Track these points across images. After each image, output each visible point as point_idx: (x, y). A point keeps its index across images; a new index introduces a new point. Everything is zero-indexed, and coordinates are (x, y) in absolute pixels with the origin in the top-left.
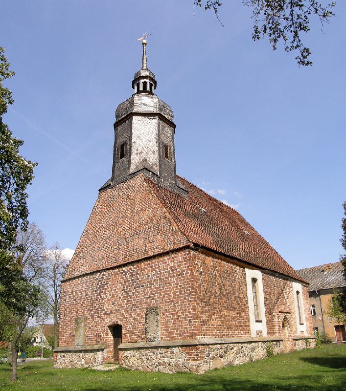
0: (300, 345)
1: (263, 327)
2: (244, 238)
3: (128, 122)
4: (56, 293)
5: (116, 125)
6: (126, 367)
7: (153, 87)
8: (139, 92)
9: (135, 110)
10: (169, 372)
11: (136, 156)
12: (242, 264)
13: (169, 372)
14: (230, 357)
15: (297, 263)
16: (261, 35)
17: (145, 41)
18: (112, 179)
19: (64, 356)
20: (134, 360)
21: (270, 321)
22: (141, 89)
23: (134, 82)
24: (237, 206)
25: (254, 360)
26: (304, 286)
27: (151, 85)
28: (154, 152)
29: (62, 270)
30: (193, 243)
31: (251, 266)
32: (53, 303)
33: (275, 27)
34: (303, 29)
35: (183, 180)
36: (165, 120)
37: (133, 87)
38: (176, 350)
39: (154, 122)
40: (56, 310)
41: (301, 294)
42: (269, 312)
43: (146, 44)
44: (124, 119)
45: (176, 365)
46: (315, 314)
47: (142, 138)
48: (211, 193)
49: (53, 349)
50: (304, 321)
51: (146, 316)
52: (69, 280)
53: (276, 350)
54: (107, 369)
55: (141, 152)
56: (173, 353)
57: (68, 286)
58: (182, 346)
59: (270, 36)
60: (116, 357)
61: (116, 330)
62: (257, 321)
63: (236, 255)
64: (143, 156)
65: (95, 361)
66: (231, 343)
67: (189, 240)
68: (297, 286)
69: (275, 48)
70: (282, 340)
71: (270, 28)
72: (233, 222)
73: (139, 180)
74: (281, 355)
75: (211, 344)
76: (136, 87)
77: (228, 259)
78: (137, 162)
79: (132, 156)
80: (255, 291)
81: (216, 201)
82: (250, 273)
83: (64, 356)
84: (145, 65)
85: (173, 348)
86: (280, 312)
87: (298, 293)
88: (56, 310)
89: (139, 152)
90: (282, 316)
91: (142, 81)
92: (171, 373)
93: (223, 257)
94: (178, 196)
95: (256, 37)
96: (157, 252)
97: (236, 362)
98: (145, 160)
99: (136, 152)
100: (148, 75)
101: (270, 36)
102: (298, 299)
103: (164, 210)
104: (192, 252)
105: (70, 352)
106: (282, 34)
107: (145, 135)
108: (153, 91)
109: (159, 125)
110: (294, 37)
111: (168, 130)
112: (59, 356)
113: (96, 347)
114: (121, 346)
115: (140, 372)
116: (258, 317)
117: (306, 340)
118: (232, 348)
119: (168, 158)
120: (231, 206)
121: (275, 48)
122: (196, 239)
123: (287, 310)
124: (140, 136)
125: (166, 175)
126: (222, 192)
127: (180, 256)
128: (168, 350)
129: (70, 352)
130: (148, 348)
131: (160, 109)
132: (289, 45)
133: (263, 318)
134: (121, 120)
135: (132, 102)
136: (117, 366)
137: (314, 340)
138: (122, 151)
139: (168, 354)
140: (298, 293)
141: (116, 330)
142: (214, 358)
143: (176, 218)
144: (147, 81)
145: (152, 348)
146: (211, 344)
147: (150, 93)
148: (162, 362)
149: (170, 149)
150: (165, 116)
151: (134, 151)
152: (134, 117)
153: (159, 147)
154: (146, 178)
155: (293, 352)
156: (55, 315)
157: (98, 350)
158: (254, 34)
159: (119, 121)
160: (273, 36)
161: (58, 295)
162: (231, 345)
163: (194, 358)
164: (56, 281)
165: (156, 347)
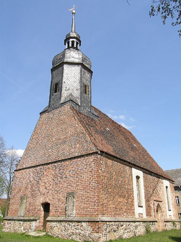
0: (169, 226)
1: (143, 211)
2: (133, 148)
3: (60, 68)
4: (10, 177)
5: (53, 70)
6: (50, 234)
7: (79, 45)
8: (69, 48)
9: (65, 60)
10: (79, 240)
11: (65, 91)
12: (130, 165)
13: (79, 240)
14: (121, 231)
15: (165, 164)
16: (155, 13)
17: (74, 11)
18: (49, 106)
19: (10, 223)
20: (57, 229)
21: (148, 207)
22: (70, 45)
23: (65, 41)
24: (131, 127)
25: (137, 235)
26: (171, 183)
27: (77, 43)
28: (77, 90)
29: (16, 163)
30: (100, 150)
31: (136, 167)
32: (7, 184)
33: (167, 7)
34: (164, 23)
35: (96, 109)
36: (85, 67)
37: (65, 44)
38: (84, 224)
39: (78, 69)
40: (9, 189)
41: (169, 188)
42: (147, 201)
43: (75, 13)
44: (58, 66)
45: (84, 236)
46: (179, 203)
47: (70, 79)
48: (114, 118)
49: (4, 216)
50: (171, 208)
51: (66, 198)
52: (20, 170)
53: (153, 228)
54: (37, 235)
55: (69, 89)
56: (82, 226)
57: (18, 174)
58: (88, 222)
59: (162, 14)
60: (44, 226)
61: (46, 207)
62: (139, 206)
63: (127, 159)
64: (70, 91)
65: (30, 228)
66: (121, 222)
67: (97, 149)
68: (166, 183)
69: (164, 23)
70: (156, 222)
71: (162, 8)
72: (126, 139)
73: (67, 107)
74: (156, 232)
75: (108, 222)
76: (67, 44)
77: (122, 161)
78: (66, 96)
79: (63, 91)
80: (138, 186)
81: (116, 123)
82: (136, 172)
83: (10, 223)
84: (73, 29)
85: (83, 223)
86: (155, 201)
87: (167, 187)
88: (9, 189)
89: (67, 89)
90: (156, 204)
91: (71, 40)
92: (80, 241)
93: (119, 160)
94: (92, 120)
95: (152, 13)
96: (77, 154)
97: (125, 236)
98: (71, 95)
99: (65, 89)
100: (76, 36)
101: (162, 14)
102: (167, 192)
103: (82, 128)
104: (99, 156)
105: (15, 220)
106: (171, 13)
107: (71, 77)
108: (79, 47)
109: (81, 71)
110: (179, 15)
111: (88, 75)
112: (6, 222)
113: (32, 218)
114: (49, 218)
115: (59, 239)
116: (140, 203)
117: (174, 222)
118: (122, 226)
119: (86, 94)
120: (126, 127)
121: (164, 23)
122: (101, 147)
123: (159, 200)
124: (69, 78)
125: (85, 105)
126: (122, 117)
127: (91, 158)
128: (80, 224)
129: (15, 220)
130: (66, 221)
131: (83, 60)
132: (175, 21)
133: (143, 203)
134: (56, 66)
135: (63, 55)
136: (44, 233)
137: (179, 223)
138: (56, 87)
139: (79, 227)
140: (167, 187)
141: (46, 207)
142: (109, 232)
143: (90, 134)
144: (75, 40)
145: (69, 221)
146: (108, 222)
147: (77, 49)
148: (74, 232)
149: (88, 88)
150: (86, 65)
151: (64, 89)
152: (64, 65)
153: (81, 86)
154: (71, 107)
155: (165, 231)
156: (8, 193)
157: (33, 220)
158: (151, 12)
159: (54, 68)
160: (164, 14)
161: (12, 179)
162: (122, 223)
163: (96, 231)
164: (11, 169)
165: (71, 221)
